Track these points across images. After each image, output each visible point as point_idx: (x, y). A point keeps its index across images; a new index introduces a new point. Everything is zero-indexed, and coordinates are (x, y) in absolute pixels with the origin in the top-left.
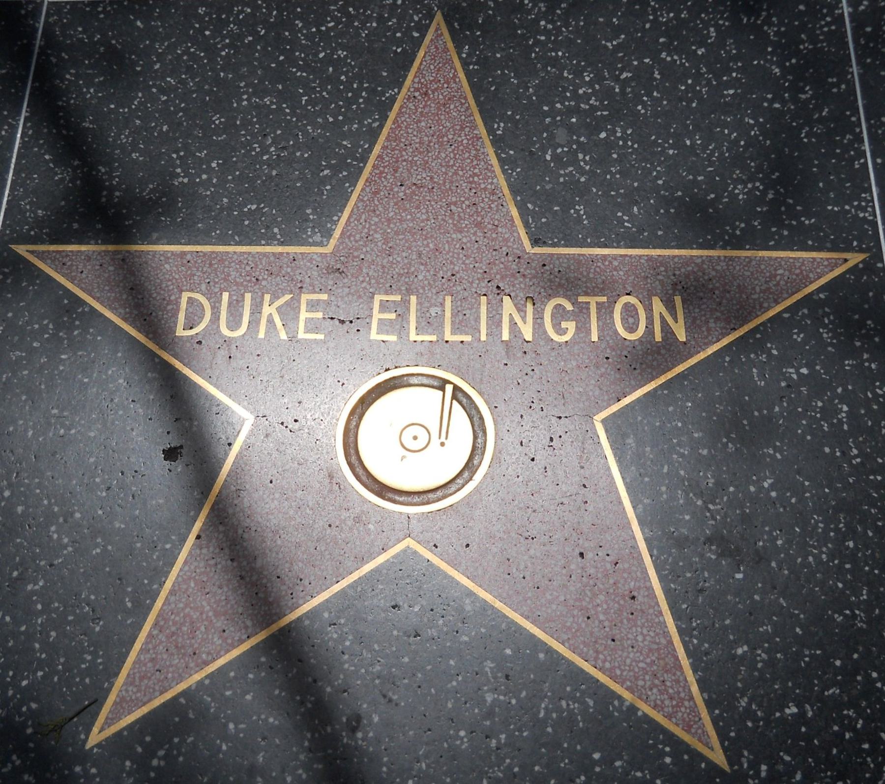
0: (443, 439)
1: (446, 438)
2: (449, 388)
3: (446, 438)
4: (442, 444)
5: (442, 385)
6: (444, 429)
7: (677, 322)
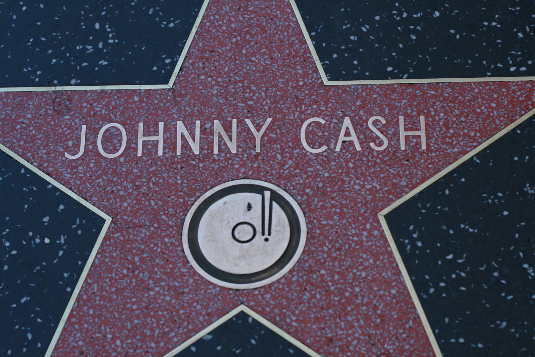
0: (266, 236)
1: (269, 234)
2: (267, 194)
3: (269, 234)
4: (266, 240)
5: (260, 190)
6: (266, 228)
7: (182, 133)
